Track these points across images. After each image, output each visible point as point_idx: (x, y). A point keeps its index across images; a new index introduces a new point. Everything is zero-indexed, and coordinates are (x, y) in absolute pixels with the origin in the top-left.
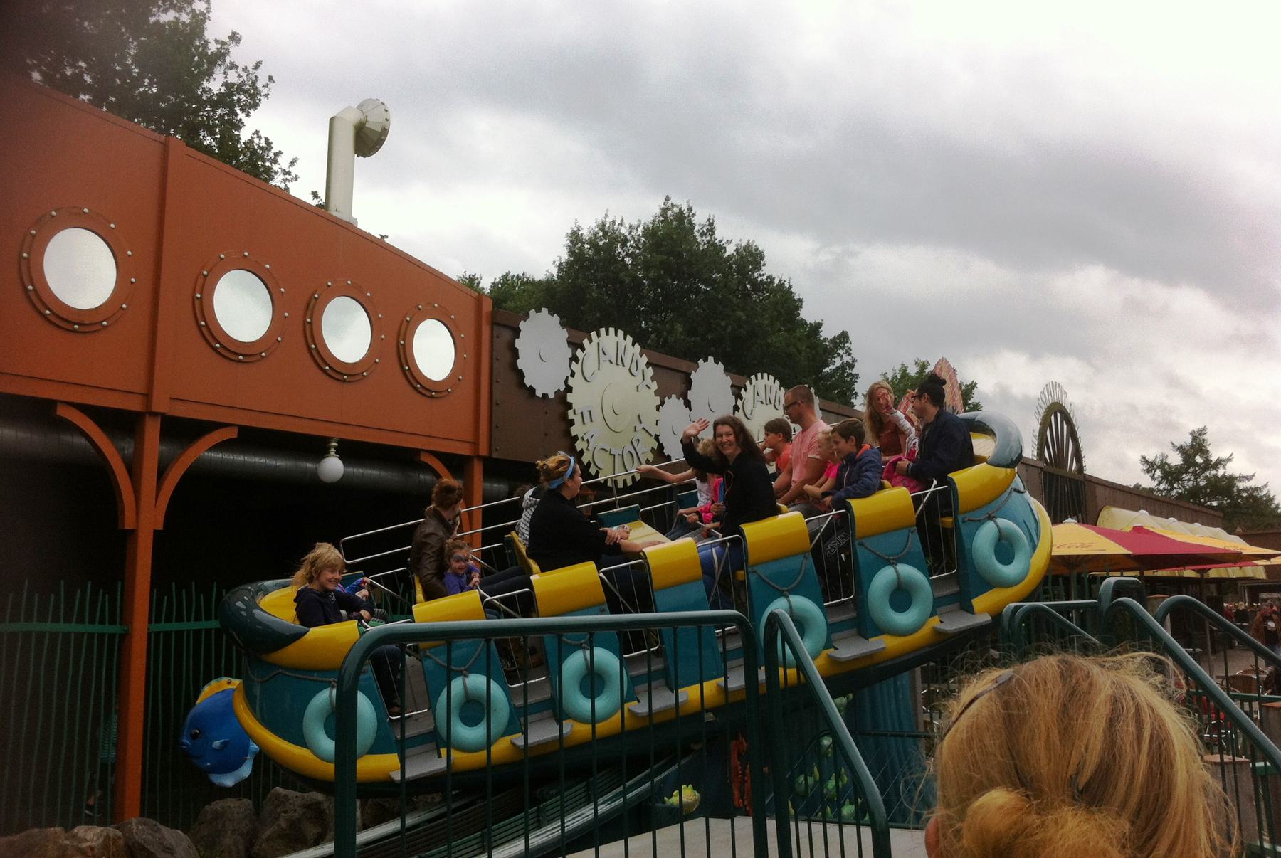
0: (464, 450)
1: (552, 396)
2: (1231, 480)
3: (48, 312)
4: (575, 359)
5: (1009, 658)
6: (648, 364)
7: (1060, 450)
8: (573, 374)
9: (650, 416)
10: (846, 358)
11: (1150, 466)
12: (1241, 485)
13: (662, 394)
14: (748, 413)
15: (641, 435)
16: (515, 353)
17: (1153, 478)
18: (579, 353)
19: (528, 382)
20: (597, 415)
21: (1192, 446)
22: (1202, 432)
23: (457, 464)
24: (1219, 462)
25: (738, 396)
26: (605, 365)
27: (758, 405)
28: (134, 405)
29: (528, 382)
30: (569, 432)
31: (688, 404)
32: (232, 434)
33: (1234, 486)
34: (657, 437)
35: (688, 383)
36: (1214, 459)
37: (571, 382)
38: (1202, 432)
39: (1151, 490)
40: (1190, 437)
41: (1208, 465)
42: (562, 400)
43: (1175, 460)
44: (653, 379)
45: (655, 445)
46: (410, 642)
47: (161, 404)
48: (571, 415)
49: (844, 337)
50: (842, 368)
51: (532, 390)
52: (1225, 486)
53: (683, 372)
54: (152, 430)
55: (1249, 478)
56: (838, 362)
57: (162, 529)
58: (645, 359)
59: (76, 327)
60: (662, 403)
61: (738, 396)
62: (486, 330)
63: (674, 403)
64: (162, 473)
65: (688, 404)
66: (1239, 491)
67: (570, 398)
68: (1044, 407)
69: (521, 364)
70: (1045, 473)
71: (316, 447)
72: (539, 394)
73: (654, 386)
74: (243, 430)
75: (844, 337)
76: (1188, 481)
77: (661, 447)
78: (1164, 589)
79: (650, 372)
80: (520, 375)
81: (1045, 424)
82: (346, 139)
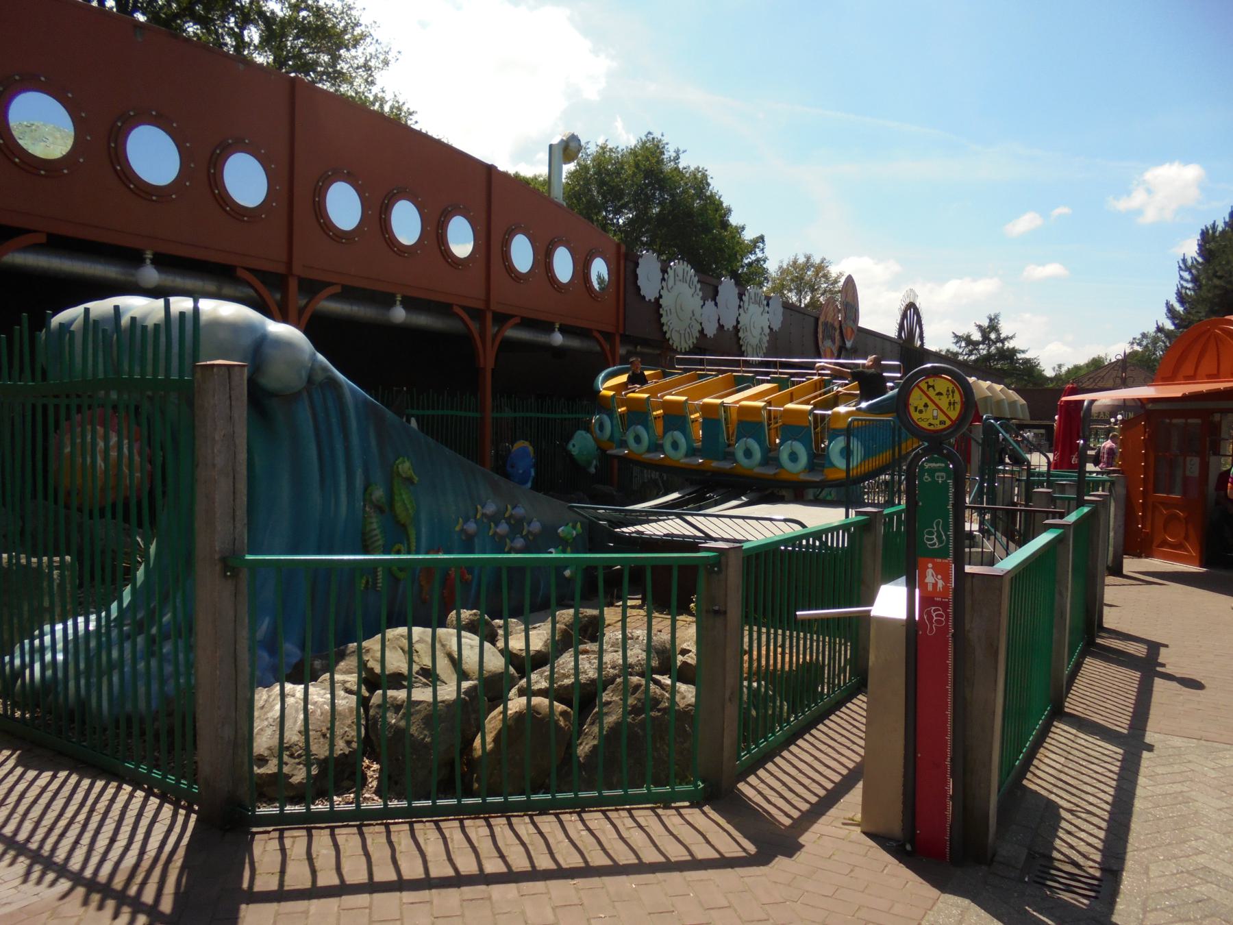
0: (610, 329)
1: (653, 300)
2: (1014, 351)
4: (663, 279)
5: (348, 685)
6: (698, 281)
10: (760, 255)
11: (958, 339)
12: (1019, 356)
13: (704, 299)
14: (670, 287)
15: (694, 323)
17: (960, 347)
18: (666, 276)
21: (989, 327)
22: (996, 316)
23: (608, 336)
25: (741, 299)
26: (677, 282)
27: (751, 304)
28: (281, 269)
29: (642, 293)
31: (716, 304)
32: (338, 289)
34: (701, 324)
35: (716, 293)
36: (1003, 336)
37: (662, 292)
38: (996, 316)
39: (956, 354)
40: (988, 320)
41: (999, 340)
42: (657, 304)
43: (977, 336)
47: (494, 306)
48: (661, 311)
49: (761, 239)
50: (758, 260)
51: (644, 297)
54: (489, 316)
55: (1023, 352)
56: (753, 257)
58: (696, 279)
59: (17, 160)
61: (741, 299)
63: (710, 303)
64: (493, 340)
65: (716, 304)
66: (1018, 359)
67: (661, 301)
68: (904, 305)
69: (639, 283)
70: (902, 347)
71: (387, 301)
72: (647, 299)
74: (344, 287)
75: (761, 239)
76: (983, 350)
77: (703, 329)
79: (699, 286)
80: (638, 289)
81: (904, 316)
82: (558, 154)
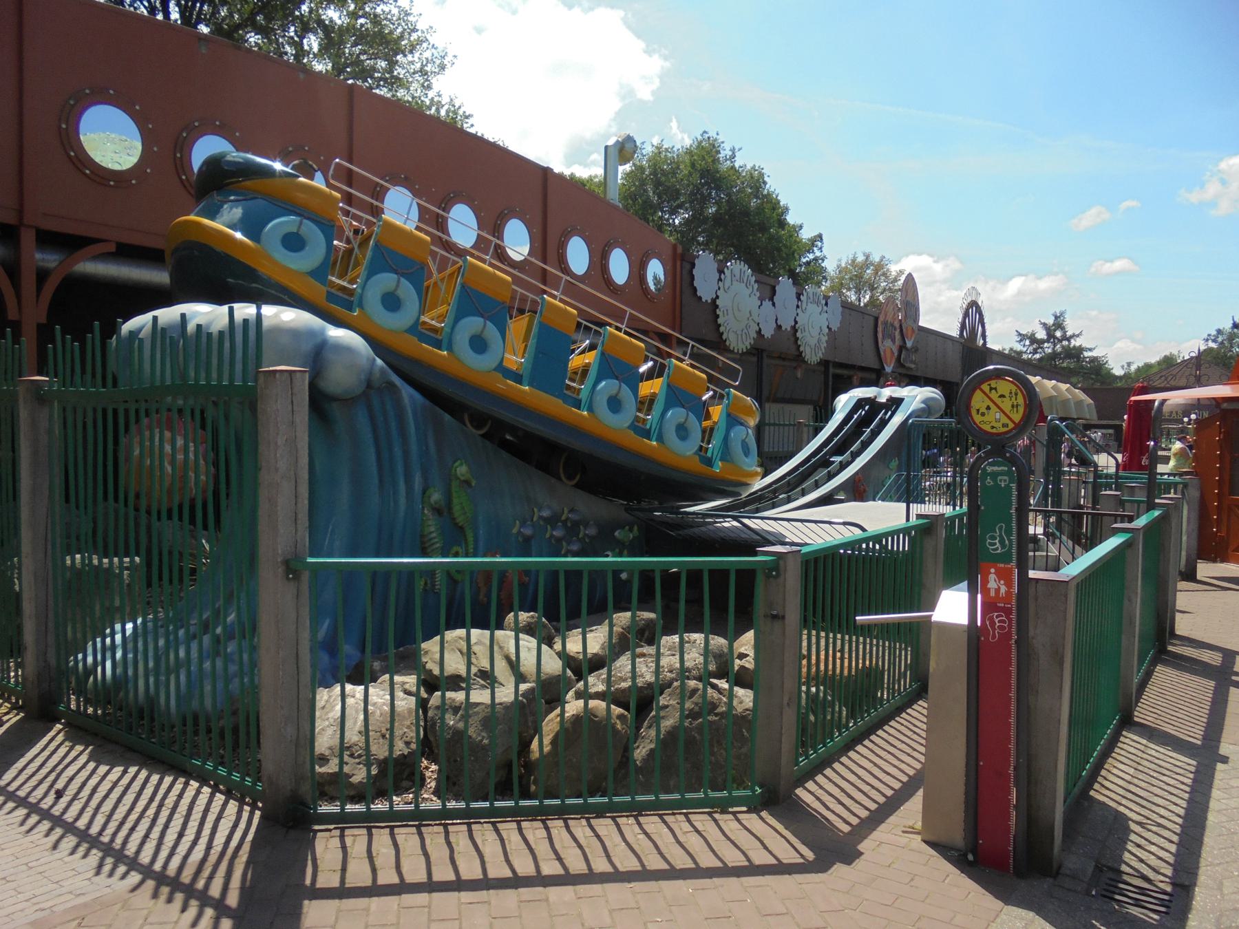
1: (709, 301)
2: (1080, 350)
3: (72, 154)
4: (720, 279)
6: (756, 281)
7: (973, 328)
8: (719, 289)
9: (755, 311)
10: (818, 254)
11: (1022, 337)
12: (1086, 354)
13: (761, 299)
16: (692, 278)
17: (1024, 346)
19: (699, 294)
20: (730, 312)
22: (1062, 314)
24: (1073, 336)
25: (799, 299)
26: (734, 283)
27: (809, 304)
30: (717, 321)
31: (774, 304)
33: (1082, 353)
34: (758, 324)
38: (1062, 314)
41: (1065, 338)
42: (714, 304)
44: (757, 290)
45: (758, 329)
46: (512, 435)
48: (718, 312)
49: (820, 237)
50: (816, 259)
51: (700, 298)
52: (1076, 353)
53: (769, 285)
56: (811, 256)
57: (45, 322)
58: (753, 279)
60: (761, 304)
62: (678, 263)
63: (767, 303)
65: (774, 304)
66: (1084, 357)
67: (718, 302)
73: (758, 294)
75: (820, 237)
76: (1048, 348)
77: (760, 329)
78: (536, 313)
82: (614, 154)
